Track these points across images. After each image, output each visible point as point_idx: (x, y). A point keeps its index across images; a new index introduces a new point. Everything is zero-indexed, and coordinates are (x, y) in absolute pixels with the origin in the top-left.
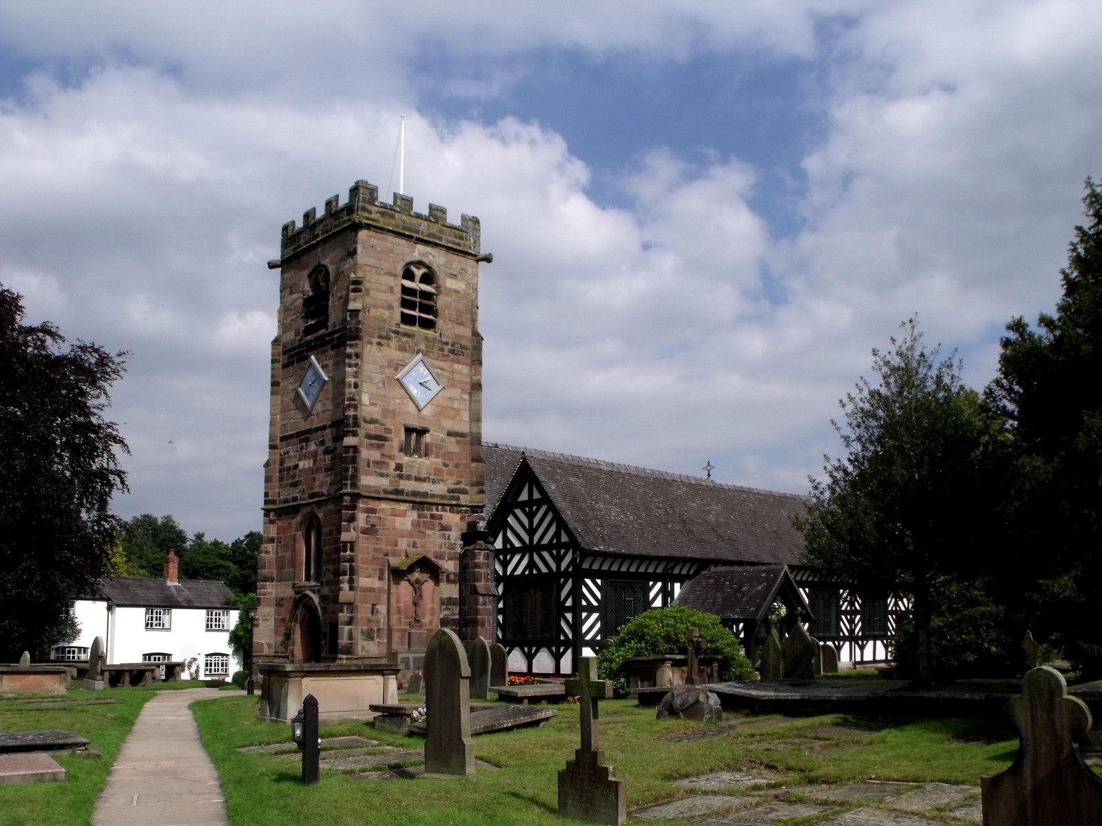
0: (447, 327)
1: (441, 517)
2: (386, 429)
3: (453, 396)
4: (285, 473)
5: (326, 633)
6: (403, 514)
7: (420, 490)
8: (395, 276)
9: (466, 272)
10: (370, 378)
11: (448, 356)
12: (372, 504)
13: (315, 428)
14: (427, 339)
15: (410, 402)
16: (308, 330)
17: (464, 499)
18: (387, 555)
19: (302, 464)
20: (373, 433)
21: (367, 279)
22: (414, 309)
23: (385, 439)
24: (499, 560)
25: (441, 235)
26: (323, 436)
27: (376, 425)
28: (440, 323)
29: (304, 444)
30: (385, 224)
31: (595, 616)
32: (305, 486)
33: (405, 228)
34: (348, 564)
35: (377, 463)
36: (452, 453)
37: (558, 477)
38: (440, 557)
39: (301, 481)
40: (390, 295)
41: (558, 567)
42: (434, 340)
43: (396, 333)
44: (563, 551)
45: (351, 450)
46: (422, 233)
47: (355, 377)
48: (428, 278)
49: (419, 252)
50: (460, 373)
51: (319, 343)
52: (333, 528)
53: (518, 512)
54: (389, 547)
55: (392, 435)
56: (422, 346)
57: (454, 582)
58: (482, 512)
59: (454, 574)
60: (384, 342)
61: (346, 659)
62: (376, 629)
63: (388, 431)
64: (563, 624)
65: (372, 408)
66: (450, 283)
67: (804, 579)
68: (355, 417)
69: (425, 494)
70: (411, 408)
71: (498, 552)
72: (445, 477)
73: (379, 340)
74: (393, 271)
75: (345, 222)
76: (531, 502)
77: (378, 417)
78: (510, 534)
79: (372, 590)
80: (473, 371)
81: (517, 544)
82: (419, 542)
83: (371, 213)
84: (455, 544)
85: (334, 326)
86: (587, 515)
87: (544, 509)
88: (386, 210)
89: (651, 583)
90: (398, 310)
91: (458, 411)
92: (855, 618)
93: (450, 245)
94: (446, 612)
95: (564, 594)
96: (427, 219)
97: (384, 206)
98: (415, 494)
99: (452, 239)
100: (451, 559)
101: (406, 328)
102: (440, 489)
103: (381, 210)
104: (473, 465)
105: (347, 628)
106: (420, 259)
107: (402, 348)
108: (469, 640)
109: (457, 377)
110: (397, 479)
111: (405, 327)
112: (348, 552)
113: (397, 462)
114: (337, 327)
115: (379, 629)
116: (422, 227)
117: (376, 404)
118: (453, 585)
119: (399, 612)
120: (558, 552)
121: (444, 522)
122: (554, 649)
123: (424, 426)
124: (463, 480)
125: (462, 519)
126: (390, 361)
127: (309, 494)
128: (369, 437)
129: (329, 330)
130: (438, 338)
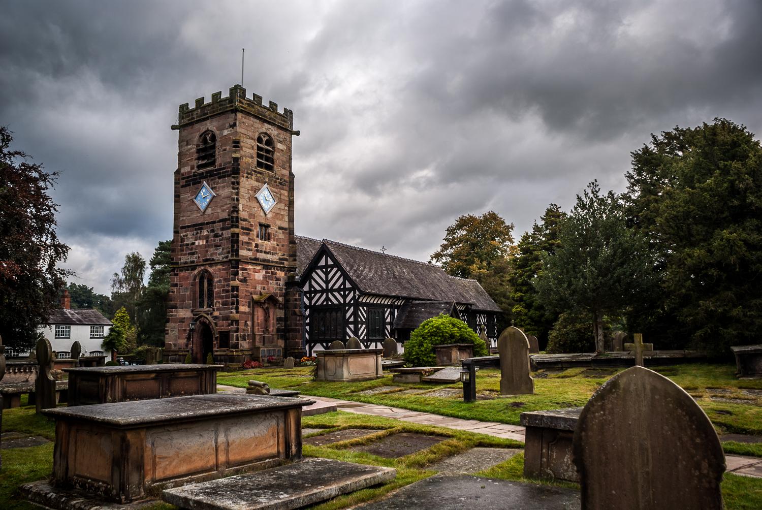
0: (279, 171)
2: (251, 224)
3: (281, 207)
6: (259, 272)
7: (266, 258)
8: (254, 140)
10: (243, 196)
11: (279, 186)
16: (199, 167)
18: (251, 294)
20: (245, 226)
21: (241, 141)
23: (250, 230)
24: (307, 297)
29: (199, 231)
31: (364, 326)
32: (200, 255)
34: (235, 299)
36: (280, 238)
39: (197, 252)
43: (255, 171)
44: (347, 292)
45: (236, 235)
48: (270, 142)
50: (284, 195)
51: (209, 174)
53: (319, 271)
56: (267, 180)
58: (295, 271)
59: (283, 305)
60: (249, 176)
62: (247, 334)
63: (252, 226)
64: (348, 330)
66: (279, 146)
68: (237, 217)
69: (269, 261)
70: (262, 214)
71: (306, 293)
74: (253, 137)
75: (227, 107)
76: (327, 266)
80: (290, 194)
82: (266, 286)
83: (243, 103)
85: (220, 165)
88: (250, 104)
89: (386, 309)
95: (348, 315)
96: (268, 109)
97: (249, 100)
98: (264, 260)
100: (280, 296)
101: (259, 169)
102: (275, 258)
103: (248, 102)
105: (235, 334)
107: (257, 180)
108: (291, 340)
118: (281, 311)
119: (258, 326)
120: (344, 293)
121: (278, 276)
122: (325, 344)
125: (285, 274)
127: (203, 260)
128: (243, 228)
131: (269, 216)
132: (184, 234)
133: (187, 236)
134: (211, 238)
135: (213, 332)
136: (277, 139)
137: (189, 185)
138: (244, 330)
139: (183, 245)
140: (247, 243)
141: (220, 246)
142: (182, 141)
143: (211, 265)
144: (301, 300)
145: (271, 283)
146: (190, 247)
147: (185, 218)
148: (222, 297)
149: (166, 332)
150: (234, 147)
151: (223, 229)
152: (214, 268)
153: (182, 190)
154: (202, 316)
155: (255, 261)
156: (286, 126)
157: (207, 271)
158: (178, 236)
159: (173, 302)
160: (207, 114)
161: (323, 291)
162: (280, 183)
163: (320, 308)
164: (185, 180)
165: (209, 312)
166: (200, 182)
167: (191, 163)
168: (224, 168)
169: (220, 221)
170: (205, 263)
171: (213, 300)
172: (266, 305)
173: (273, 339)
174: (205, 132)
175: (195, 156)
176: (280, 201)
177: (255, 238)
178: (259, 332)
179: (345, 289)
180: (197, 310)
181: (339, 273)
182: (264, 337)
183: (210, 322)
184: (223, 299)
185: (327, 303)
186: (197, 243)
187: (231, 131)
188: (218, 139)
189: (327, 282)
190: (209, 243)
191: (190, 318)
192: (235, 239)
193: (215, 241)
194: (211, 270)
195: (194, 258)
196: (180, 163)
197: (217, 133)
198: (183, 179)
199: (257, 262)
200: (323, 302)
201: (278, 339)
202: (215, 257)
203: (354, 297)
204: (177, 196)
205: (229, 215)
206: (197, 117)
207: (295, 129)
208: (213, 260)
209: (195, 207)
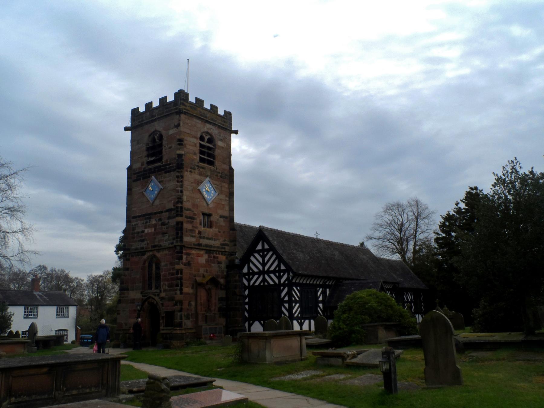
1: (217, 257)
4: (136, 235)
5: (164, 316)
6: (202, 256)
7: (209, 244)
9: (227, 138)
12: (188, 251)
13: (155, 212)
15: (204, 201)
16: (149, 163)
17: (227, 249)
19: (146, 231)
20: (188, 215)
22: (204, 155)
23: (194, 219)
25: (216, 120)
27: (190, 211)
28: (216, 163)
29: (148, 220)
32: (149, 242)
33: (201, 115)
35: (191, 230)
40: (195, 148)
41: (280, 281)
43: (198, 166)
48: (210, 141)
49: (207, 127)
53: (256, 255)
55: (196, 217)
56: (209, 174)
60: (193, 170)
61: (179, 330)
62: (190, 314)
63: (195, 215)
64: (283, 309)
67: (389, 287)
68: (181, 208)
70: (205, 204)
71: (246, 274)
73: (191, 170)
75: (172, 110)
76: (263, 250)
77: (190, 207)
78: (252, 266)
81: (256, 270)
84: (224, 271)
85: (167, 161)
87: (270, 253)
94: (221, 305)
95: (283, 294)
98: (207, 246)
99: (220, 122)
100: (222, 278)
101: (202, 164)
102: (217, 243)
104: (231, 232)
105: (179, 314)
106: (207, 131)
107: (200, 174)
110: (199, 238)
111: (202, 164)
112: (179, 275)
113: (199, 230)
114: (169, 162)
116: (208, 115)
117: (189, 201)
120: (279, 274)
123: (210, 212)
126: (195, 180)
128: (187, 217)
129: (163, 164)
130: (215, 170)
132: (135, 223)
133: (137, 224)
137: (140, 179)
138: (188, 309)
141: (166, 233)
143: (158, 251)
147: (135, 209)
150: (179, 144)
151: (169, 218)
152: (161, 253)
154: (150, 297)
155: (198, 246)
157: (154, 256)
160: (155, 116)
161: (260, 273)
162: (221, 177)
164: (136, 175)
165: (157, 294)
168: (170, 164)
170: (153, 249)
174: (154, 132)
175: (145, 153)
177: (198, 225)
179: (280, 271)
181: (274, 257)
183: (157, 303)
185: (264, 284)
188: (164, 137)
189: (264, 264)
192: (179, 227)
194: (158, 255)
195: (144, 245)
197: (164, 133)
198: (135, 174)
199: (201, 248)
202: (162, 244)
205: (174, 206)
207: (234, 128)
208: (161, 246)
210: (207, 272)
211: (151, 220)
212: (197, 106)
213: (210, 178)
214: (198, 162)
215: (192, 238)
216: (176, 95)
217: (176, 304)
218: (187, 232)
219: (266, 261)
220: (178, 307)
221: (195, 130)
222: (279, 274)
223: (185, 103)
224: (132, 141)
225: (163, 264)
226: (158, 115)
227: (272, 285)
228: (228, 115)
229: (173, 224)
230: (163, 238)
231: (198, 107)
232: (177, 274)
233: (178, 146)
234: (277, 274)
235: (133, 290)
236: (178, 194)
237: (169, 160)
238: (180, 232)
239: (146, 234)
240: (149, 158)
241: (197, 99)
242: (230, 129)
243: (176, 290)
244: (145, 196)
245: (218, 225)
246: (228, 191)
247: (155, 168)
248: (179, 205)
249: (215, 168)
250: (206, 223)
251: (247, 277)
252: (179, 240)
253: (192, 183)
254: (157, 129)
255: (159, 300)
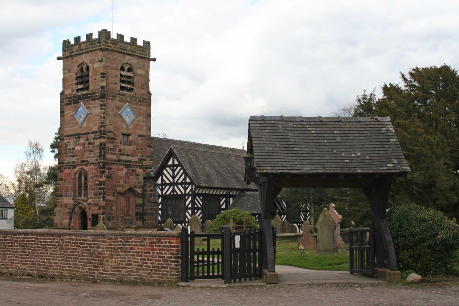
0: (138, 91)
1: (136, 171)
2: (115, 135)
4: (68, 151)
6: (121, 170)
8: (118, 70)
14: (130, 96)
15: (124, 123)
16: (78, 90)
18: (116, 186)
19: (76, 148)
20: (110, 137)
23: (115, 139)
24: (159, 188)
26: (88, 137)
27: (112, 133)
28: (135, 89)
29: (78, 139)
30: (114, 48)
31: (200, 211)
32: (78, 157)
36: (140, 144)
37: (185, 155)
38: (136, 187)
41: (185, 192)
42: (133, 96)
43: (119, 94)
46: (128, 50)
47: (104, 114)
52: (94, 175)
53: (168, 169)
54: (117, 183)
55: (117, 137)
56: (128, 100)
57: (141, 197)
58: (151, 168)
59: (141, 194)
60: (114, 98)
62: (111, 216)
63: (116, 135)
64: (187, 214)
65: (110, 126)
69: (130, 161)
70: (124, 126)
71: (159, 185)
72: (137, 154)
73: (112, 98)
75: (97, 46)
76: (173, 165)
77: (112, 130)
78: (164, 178)
79: (110, 201)
80: (148, 108)
81: (167, 182)
83: (108, 43)
85: (92, 90)
86: (197, 171)
87: (179, 168)
89: (221, 198)
90: (119, 84)
91: (142, 126)
92: (307, 213)
93: (139, 55)
94: (138, 210)
95: (187, 203)
97: (113, 40)
98: (126, 161)
99: (139, 52)
100: (139, 188)
101: (122, 92)
102: (135, 159)
103: (113, 42)
105: (102, 216)
107: (121, 101)
109: (141, 112)
112: (102, 186)
115: (113, 217)
120: (185, 186)
121: (137, 172)
124: (144, 155)
125: (144, 171)
131: (130, 127)
132: (67, 141)
133: (69, 142)
134: (86, 145)
135: (87, 214)
136: (137, 67)
137: (70, 104)
138: (110, 213)
139: (67, 150)
140: (113, 149)
141: (92, 151)
142: (66, 69)
143: (86, 165)
144: (155, 190)
145: (131, 178)
146: (71, 151)
147: (68, 129)
148: (94, 189)
149: (55, 214)
150: (102, 77)
151: (95, 139)
152: (88, 167)
153: (66, 107)
154: (79, 203)
156: (145, 55)
157: (84, 169)
158: (63, 142)
159: (60, 192)
160: (82, 50)
161: (171, 184)
162: (140, 101)
163: (168, 197)
164: (67, 100)
165: (85, 200)
166: (78, 102)
167: (71, 87)
168: (95, 93)
169: (93, 133)
170: (82, 164)
171: (88, 191)
172: (127, 195)
173: (132, 220)
174: (82, 63)
175: (75, 81)
176: (140, 115)
177: (119, 144)
178: (121, 214)
179: (186, 183)
180: (76, 198)
181: (182, 171)
182: (125, 219)
183: (85, 207)
184: (94, 190)
185: (173, 193)
186: (76, 148)
187: (100, 65)
188: (91, 69)
189: (174, 177)
190: (85, 149)
191: (72, 204)
193: (89, 147)
194: (86, 169)
195: (74, 159)
196: (63, 87)
197: (90, 65)
198: (66, 99)
199: (121, 163)
200: (171, 193)
201: (137, 220)
202: (89, 159)
203: (192, 189)
204: (62, 112)
205: (98, 129)
206: (76, 52)
207: (152, 56)
208: (88, 161)
209: (75, 122)
210: (126, 183)
211: (80, 139)
212: (118, 42)
213: (129, 103)
214: (119, 91)
215: (113, 155)
216: (101, 33)
217: (99, 209)
218: (109, 150)
219: (175, 175)
220: (102, 211)
221: (116, 63)
222: (185, 186)
223: (107, 41)
224: (64, 69)
225: (90, 176)
226: (85, 49)
227: (197, 196)
228: (147, 44)
229: (97, 144)
230: (90, 155)
231: (119, 42)
232: (101, 185)
233: (102, 79)
234: (184, 186)
235: (66, 197)
236: (101, 119)
237: (94, 90)
238: (103, 151)
239: (76, 151)
240: (79, 86)
241: (118, 35)
242: (148, 57)
243: (100, 198)
244: (75, 119)
245: (137, 143)
246: (146, 113)
247: (84, 95)
248: (103, 129)
249: (134, 94)
250: (126, 142)
251: (160, 187)
252: (102, 157)
253: (113, 109)
254: (84, 62)
255: (87, 205)
